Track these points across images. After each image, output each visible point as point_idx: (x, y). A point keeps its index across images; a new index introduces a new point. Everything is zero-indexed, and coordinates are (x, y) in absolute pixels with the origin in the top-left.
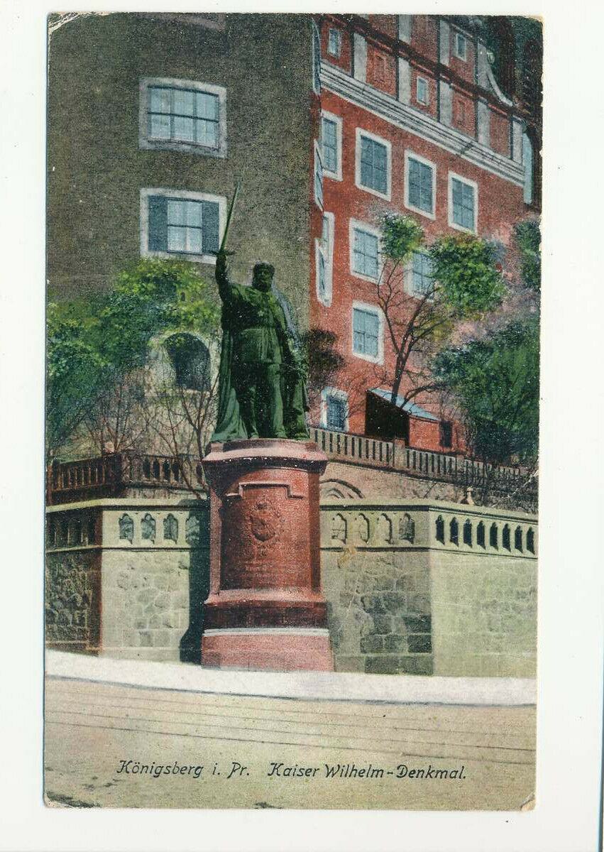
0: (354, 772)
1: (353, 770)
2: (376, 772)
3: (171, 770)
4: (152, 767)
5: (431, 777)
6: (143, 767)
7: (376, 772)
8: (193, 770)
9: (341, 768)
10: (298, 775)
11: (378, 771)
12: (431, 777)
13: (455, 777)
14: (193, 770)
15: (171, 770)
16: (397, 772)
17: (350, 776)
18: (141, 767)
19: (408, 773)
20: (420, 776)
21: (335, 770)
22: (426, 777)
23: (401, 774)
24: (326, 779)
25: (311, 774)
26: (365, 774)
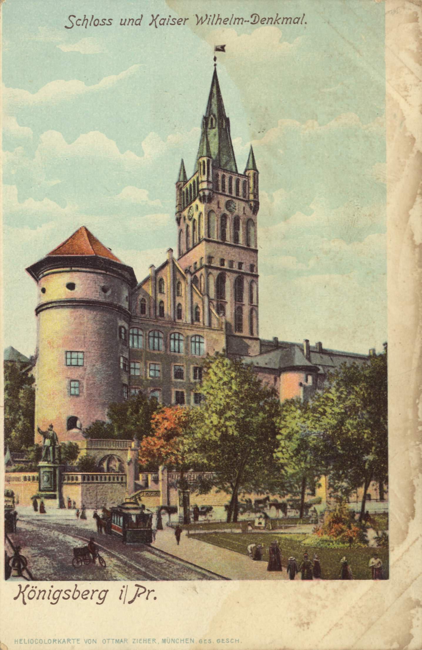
0: (219, 21)
1: (218, 19)
2: (286, 20)
3: (71, 594)
4: (50, 591)
5: (278, 23)
6: (40, 592)
7: (286, 20)
8: (96, 594)
9: (209, 17)
10: (171, 24)
11: (239, 19)
12: (278, 23)
13: (163, 24)
14: (96, 594)
15: (71, 594)
16: (252, 20)
17: (216, 24)
18: (37, 593)
19: (260, 20)
20: (284, 22)
21: (204, 19)
22: (274, 23)
23: (254, 21)
24: (179, 547)
25: (182, 23)
26: (228, 22)
